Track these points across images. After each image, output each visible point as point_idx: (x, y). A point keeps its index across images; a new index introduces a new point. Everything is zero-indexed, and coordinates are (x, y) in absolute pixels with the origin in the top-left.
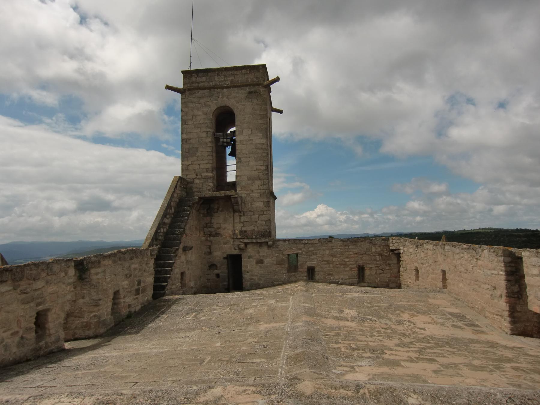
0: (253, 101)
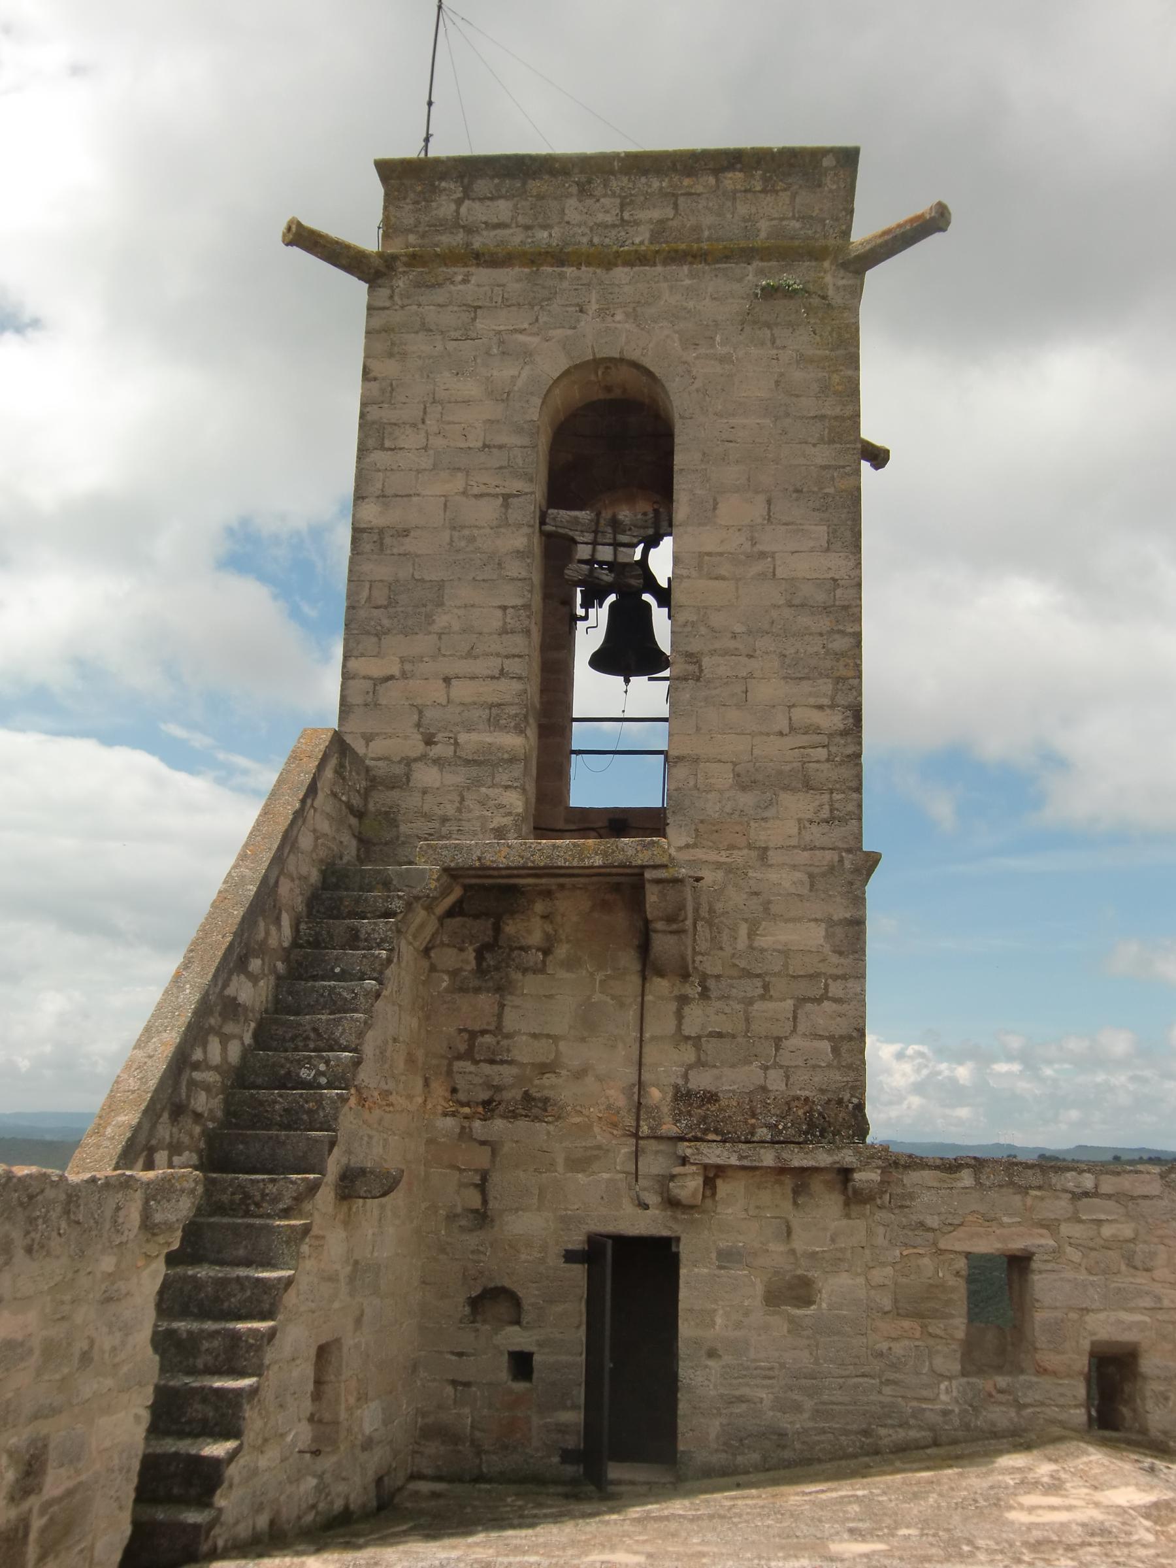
0: (778, 342)
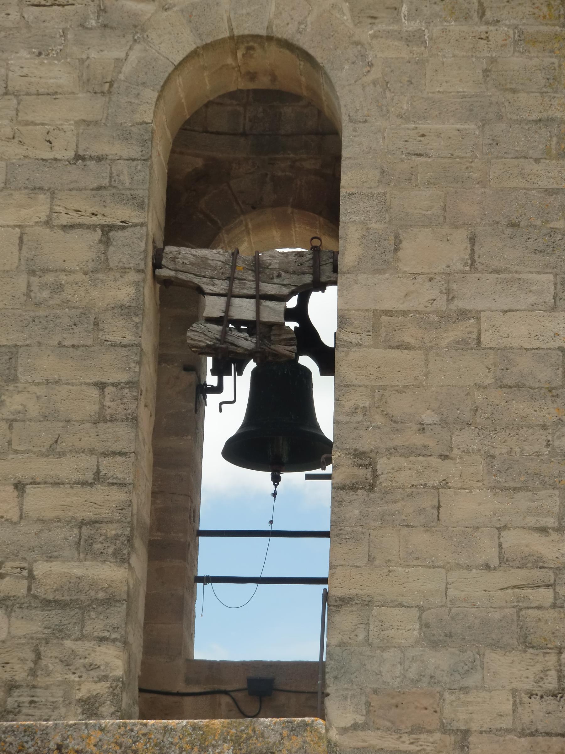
0: (488, 14)
